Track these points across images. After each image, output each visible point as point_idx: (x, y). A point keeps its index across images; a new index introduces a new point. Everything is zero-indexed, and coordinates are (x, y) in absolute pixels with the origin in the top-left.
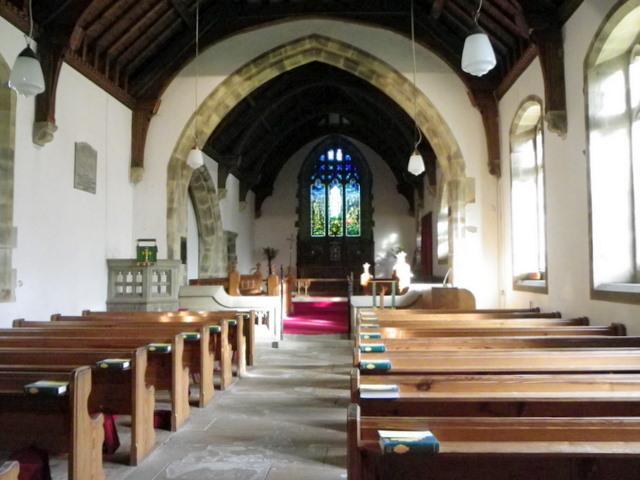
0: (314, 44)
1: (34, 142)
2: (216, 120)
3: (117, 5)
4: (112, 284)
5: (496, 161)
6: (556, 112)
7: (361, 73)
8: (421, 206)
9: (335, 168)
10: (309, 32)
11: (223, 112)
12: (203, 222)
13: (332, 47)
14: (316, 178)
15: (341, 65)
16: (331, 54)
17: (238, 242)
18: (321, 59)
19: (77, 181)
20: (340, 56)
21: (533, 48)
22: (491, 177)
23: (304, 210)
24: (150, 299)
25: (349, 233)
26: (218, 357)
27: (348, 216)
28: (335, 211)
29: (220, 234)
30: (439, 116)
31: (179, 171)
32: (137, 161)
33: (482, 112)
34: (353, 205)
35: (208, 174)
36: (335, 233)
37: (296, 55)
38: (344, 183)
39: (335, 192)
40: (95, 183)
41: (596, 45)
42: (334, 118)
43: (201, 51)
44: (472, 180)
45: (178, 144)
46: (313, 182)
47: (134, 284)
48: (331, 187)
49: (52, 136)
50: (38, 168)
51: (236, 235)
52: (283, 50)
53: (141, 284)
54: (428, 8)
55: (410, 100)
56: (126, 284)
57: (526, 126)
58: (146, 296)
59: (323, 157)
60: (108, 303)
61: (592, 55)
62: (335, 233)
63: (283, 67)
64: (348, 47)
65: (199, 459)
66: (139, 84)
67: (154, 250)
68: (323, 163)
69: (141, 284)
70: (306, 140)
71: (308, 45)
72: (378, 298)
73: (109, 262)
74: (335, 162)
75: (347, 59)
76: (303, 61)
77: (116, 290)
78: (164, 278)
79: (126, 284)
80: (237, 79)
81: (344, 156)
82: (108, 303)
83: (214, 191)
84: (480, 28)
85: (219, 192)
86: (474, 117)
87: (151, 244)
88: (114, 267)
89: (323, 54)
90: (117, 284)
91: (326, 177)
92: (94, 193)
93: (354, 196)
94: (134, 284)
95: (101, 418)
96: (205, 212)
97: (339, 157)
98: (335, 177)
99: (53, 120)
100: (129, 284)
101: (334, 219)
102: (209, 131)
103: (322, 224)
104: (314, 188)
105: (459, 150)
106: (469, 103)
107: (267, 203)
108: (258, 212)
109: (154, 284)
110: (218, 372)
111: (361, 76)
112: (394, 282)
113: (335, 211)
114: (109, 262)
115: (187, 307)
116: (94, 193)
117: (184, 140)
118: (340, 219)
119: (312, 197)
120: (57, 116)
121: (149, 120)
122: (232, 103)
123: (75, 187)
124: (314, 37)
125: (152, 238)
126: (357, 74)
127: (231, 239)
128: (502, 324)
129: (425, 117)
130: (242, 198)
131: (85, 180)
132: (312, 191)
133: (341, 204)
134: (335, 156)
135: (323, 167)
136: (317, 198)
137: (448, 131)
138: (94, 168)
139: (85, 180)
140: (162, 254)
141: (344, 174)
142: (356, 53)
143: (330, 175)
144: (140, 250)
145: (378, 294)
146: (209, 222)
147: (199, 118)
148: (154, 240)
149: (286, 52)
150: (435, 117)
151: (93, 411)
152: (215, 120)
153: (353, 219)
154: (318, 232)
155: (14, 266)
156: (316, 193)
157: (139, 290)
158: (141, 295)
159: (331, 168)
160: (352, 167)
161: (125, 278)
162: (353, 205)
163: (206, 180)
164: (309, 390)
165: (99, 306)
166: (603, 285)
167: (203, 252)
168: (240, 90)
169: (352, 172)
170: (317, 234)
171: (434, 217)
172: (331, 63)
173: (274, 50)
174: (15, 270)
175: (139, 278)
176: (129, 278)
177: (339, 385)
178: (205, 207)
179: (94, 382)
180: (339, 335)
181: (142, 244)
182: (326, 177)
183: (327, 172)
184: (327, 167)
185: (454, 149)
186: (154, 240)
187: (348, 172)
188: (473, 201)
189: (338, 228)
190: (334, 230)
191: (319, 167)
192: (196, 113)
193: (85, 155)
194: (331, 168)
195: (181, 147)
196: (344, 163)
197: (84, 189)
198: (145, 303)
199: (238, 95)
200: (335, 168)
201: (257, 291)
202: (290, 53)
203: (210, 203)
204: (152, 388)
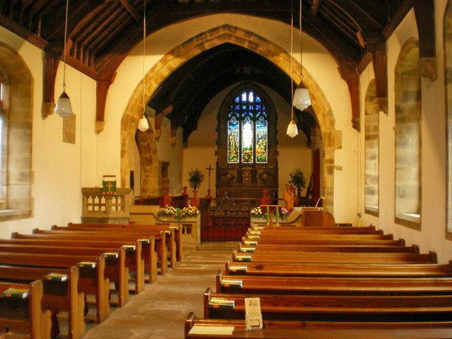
0: (227, 31)
2: (155, 86)
4: (85, 205)
5: (357, 119)
6: (379, 99)
7: (261, 52)
9: (248, 107)
10: (223, 23)
11: (160, 81)
12: (143, 154)
13: (239, 34)
15: (246, 45)
17: (170, 169)
18: (232, 41)
21: (369, 55)
23: (221, 142)
26: (170, 249)
27: (257, 147)
28: (247, 143)
30: (317, 85)
32: (100, 117)
37: (214, 39)
38: (254, 120)
39: (247, 127)
40: (74, 137)
42: (247, 70)
43: (148, 33)
45: (129, 104)
48: (244, 123)
52: (203, 36)
54: (307, 5)
56: (94, 205)
60: (83, 219)
63: (204, 47)
65: (152, 306)
68: (237, 104)
70: (221, 88)
71: (222, 32)
74: (247, 103)
75: (250, 42)
76: (218, 43)
78: (119, 201)
79: (94, 205)
80: (170, 57)
81: (255, 99)
86: (343, 86)
87: (112, 179)
88: (87, 193)
89: (233, 38)
90: (88, 205)
91: (240, 115)
93: (263, 130)
94: (100, 205)
95: (83, 295)
97: (251, 99)
98: (247, 115)
102: (150, 94)
103: (237, 153)
104: (230, 124)
109: (113, 205)
110: (159, 265)
111: (260, 54)
113: (247, 143)
118: (251, 149)
119: (229, 132)
121: (108, 87)
124: (226, 26)
125: (112, 174)
126: (257, 52)
128: (338, 238)
130: (173, 135)
131: (69, 137)
133: (252, 137)
135: (238, 107)
136: (233, 131)
137: (323, 96)
139: (69, 137)
141: (255, 112)
142: (256, 38)
143: (243, 113)
144: (104, 183)
146: (148, 155)
148: (114, 176)
151: (79, 291)
153: (261, 148)
154: (233, 160)
156: (231, 127)
160: (262, 108)
161: (100, 201)
165: (77, 220)
167: (144, 177)
170: (232, 162)
173: (197, 37)
176: (97, 200)
178: (145, 144)
179: (106, 264)
182: (240, 115)
183: (241, 111)
184: (241, 107)
186: (114, 176)
187: (258, 111)
188: (341, 148)
196: (255, 103)
200: (248, 107)
202: (208, 38)
204: (108, 280)
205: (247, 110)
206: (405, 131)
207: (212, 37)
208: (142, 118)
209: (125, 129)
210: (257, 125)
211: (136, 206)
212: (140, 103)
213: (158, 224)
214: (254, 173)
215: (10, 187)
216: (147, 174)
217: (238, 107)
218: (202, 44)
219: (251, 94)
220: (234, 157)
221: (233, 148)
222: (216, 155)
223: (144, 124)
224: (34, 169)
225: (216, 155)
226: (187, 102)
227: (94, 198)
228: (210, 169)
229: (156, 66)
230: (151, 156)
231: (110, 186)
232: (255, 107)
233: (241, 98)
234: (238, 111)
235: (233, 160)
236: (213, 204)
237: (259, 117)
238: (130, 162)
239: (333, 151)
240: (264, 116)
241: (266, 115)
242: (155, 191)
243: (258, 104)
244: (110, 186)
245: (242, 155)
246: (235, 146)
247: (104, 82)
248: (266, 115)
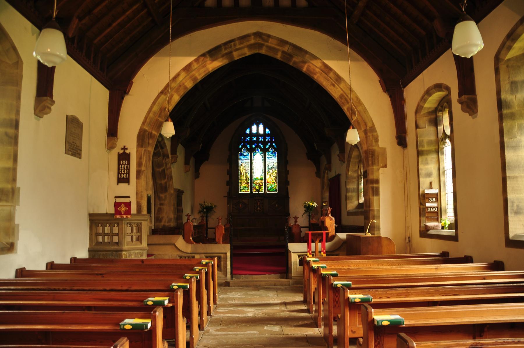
0: (259, 41)
1: (35, 114)
3: (104, 4)
4: (93, 234)
7: (295, 63)
8: (329, 169)
9: (258, 139)
10: (254, 30)
11: (182, 92)
12: (159, 182)
13: (272, 43)
15: (279, 56)
16: (270, 48)
18: (263, 51)
19: (67, 148)
20: (278, 50)
22: (399, 148)
24: (125, 247)
25: (268, 191)
27: (268, 177)
28: (258, 173)
29: (172, 192)
30: (358, 98)
31: (146, 140)
32: (112, 131)
33: (390, 97)
35: (164, 143)
36: (258, 191)
37: (243, 48)
38: (265, 151)
39: (258, 157)
40: (81, 150)
41: (508, 43)
43: (172, 41)
44: (385, 149)
46: (241, 150)
47: (112, 234)
49: (50, 109)
50: (38, 136)
51: (182, 192)
52: (232, 44)
53: (117, 235)
55: (334, 85)
56: (104, 234)
57: (429, 108)
58: (122, 244)
59: (248, 131)
61: (503, 52)
62: (258, 191)
63: (232, 57)
64: (286, 43)
66: (114, 67)
67: (128, 205)
68: (248, 135)
69: (117, 235)
71: (252, 41)
72: (313, 245)
73: (90, 215)
74: (258, 135)
75: (283, 52)
76: (247, 52)
77: (97, 239)
79: (104, 234)
81: (265, 131)
82: (89, 251)
83: (168, 157)
84: (468, 16)
85: (172, 158)
86: (385, 100)
87: (127, 200)
88: (96, 220)
91: (251, 146)
92: (80, 158)
93: (273, 161)
97: (261, 131)
99: (51, 96)
104: (241, 155)
105: (373, 125)
106: (380, 89)
107: (205, 169)
108: (197, 175)
112: (324, 232)
113: (258, 173)
114: (90, 215)
115: (153, 253)
116: (80, 158)
117: (151, 115)
118: (261, 179)
119: (240, 163)
120: (54, 93)
122: (190, 85)
123: (65, 153)
124: (258, 34)
127: (179, 194)
129: (346, 99)
130: (187, 163)
131: (74, 148)
134: (258, 130)
135: (248, 138)
136: (243, 162)
137: (365, 110)
138: (80, 138)
139: (74, 148)
140: (134, 209)
141: (265, 143)
143: (254, 145)
144: (117, 205)
145: (313, 242)
146: (163, 182)
147: (163, 97)
148: (129, 197)
149: (235, 45)
150: (355, 99)
152: (176, 98)
154: (244, 189)
155: (17, 222)
156: (242, 158)
157: (116, 239)
158: (117, 243)
159: (255, 139)
160: (271, 139)
161: (112, 230)
163: (162, 148)
164: (277, 329)
165: (83, 254)
166: (516, 235)
168: (197, 75)
169: (271, 142)
171: (343, 179)
172: (271, 54)
173: (225, 44)
174: (18, 225)
175: (116, 230)
176: (107, 229)
177: (300, 323)
178: (161, 169)
180: (279, 275)
181: (119, 200)
182: (251, 146)
183: (251, 142)
184: (251, 139)
185: (369, 125)
186: (129, 197)
187: (268, 142)
189: (260, 186)
190: (257, 187)
191: (245, 138)
192: (162, 92)
193: (73, 125)
194: (255, 139)
195: (148, 120)
196: (265, 135)
197: (72, 155)
198: (121, 251)
199: (196, 79)
202: (238, 47)
203: (164, 167)
205: (258, 142)
206: (515, 130)
207: (241, 46)
208: (167, 120)
209: (142, 146)
210: (267, 156)
211: (153, 236)
212: (159, 117)
213: (181, 257)
214: (117, 251)
216: (162, 202)
217: (248, 138)
218: (231, 52)
219: (261, 126)
220: (245, 187)
221: (243, 178)
222: (227, 185)
223: (169, 130)
224: (18, 184)
225: (227, 185)
226: (206, 123)
227: (104, 227)
229: (178, 75)
230: (166, 183)
231: (123, 209)
232: (265, 139)
234: (248, 142)
235: (244, 189)
237: (269, 148)
238: (147, 183)
239: (378, 169)
240: (273, 147)
241: (275, 147)
242: (169, 221)
243: (268, 135)
244: (123, 209)
247: (118, 90)
248: (275, 147)
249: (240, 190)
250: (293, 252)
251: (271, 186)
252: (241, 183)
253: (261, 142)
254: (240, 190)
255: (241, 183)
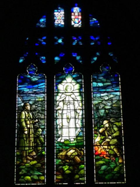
14: (82, 130)
25: (99, 180)
28: (69, 127)
34: (107, 116)
38: (86, 76)
46: (22, 69)
68: (41, 32)
81: (85, 20)
91: (50, 60)
96: (60, 128)
97: (76, 21)
100: (27, 147)
101: (66, 145)
103: (40, 158)
104: (24, 81)
113: (69, 127)
118: (77, 147)
132: (19, 87)
134: (68, 18)
136: (29, 97)
141: (86, 52)
162: (107, 116)
182: (50, 60)
183: (52, 50)
184: (51, 41)
200: (68, 41)
201: (41, 171)
215: (74, 109)
218: (94, 109)
220: (32, 167)
228: (69, 137)
232: (86, 41)
233: (51, 19)
234: (43, 51)
236: (108, 128)
245: (57, 162)
246: (37, 138)
249: (19, 176)
250: (78, 110)
251: (107, 164)
252: (20, 157)
253: (78, 49)
254: (19, 176)
255: (20, 157)
